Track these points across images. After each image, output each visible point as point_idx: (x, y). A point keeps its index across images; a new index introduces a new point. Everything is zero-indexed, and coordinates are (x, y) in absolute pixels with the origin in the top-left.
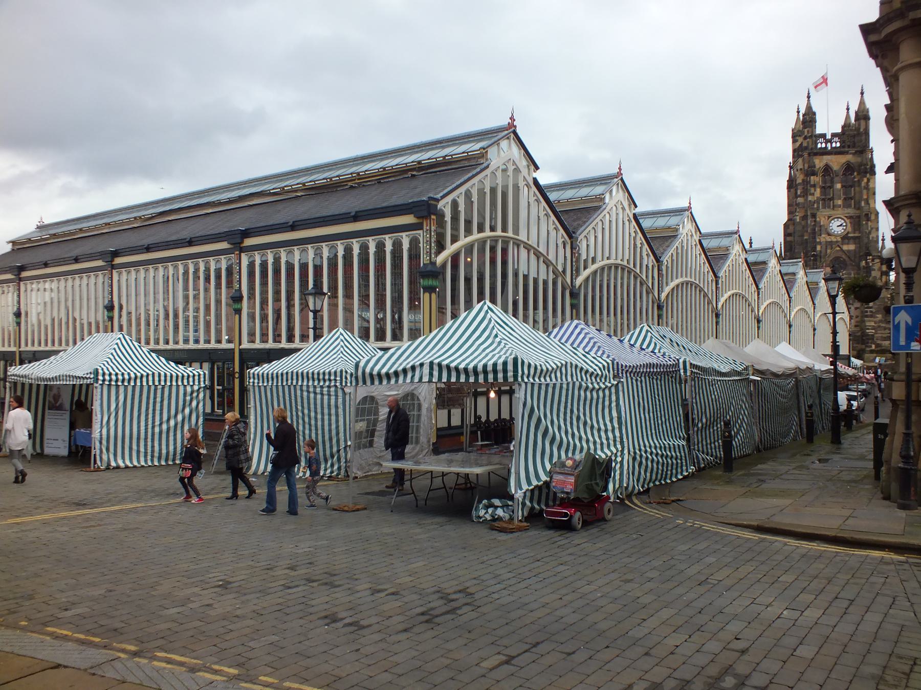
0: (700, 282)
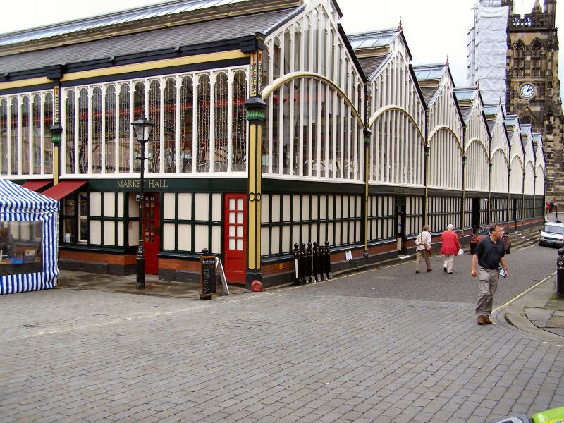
0: (405, 108)
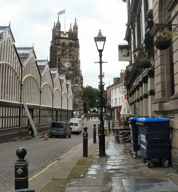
0: (11, 64)
